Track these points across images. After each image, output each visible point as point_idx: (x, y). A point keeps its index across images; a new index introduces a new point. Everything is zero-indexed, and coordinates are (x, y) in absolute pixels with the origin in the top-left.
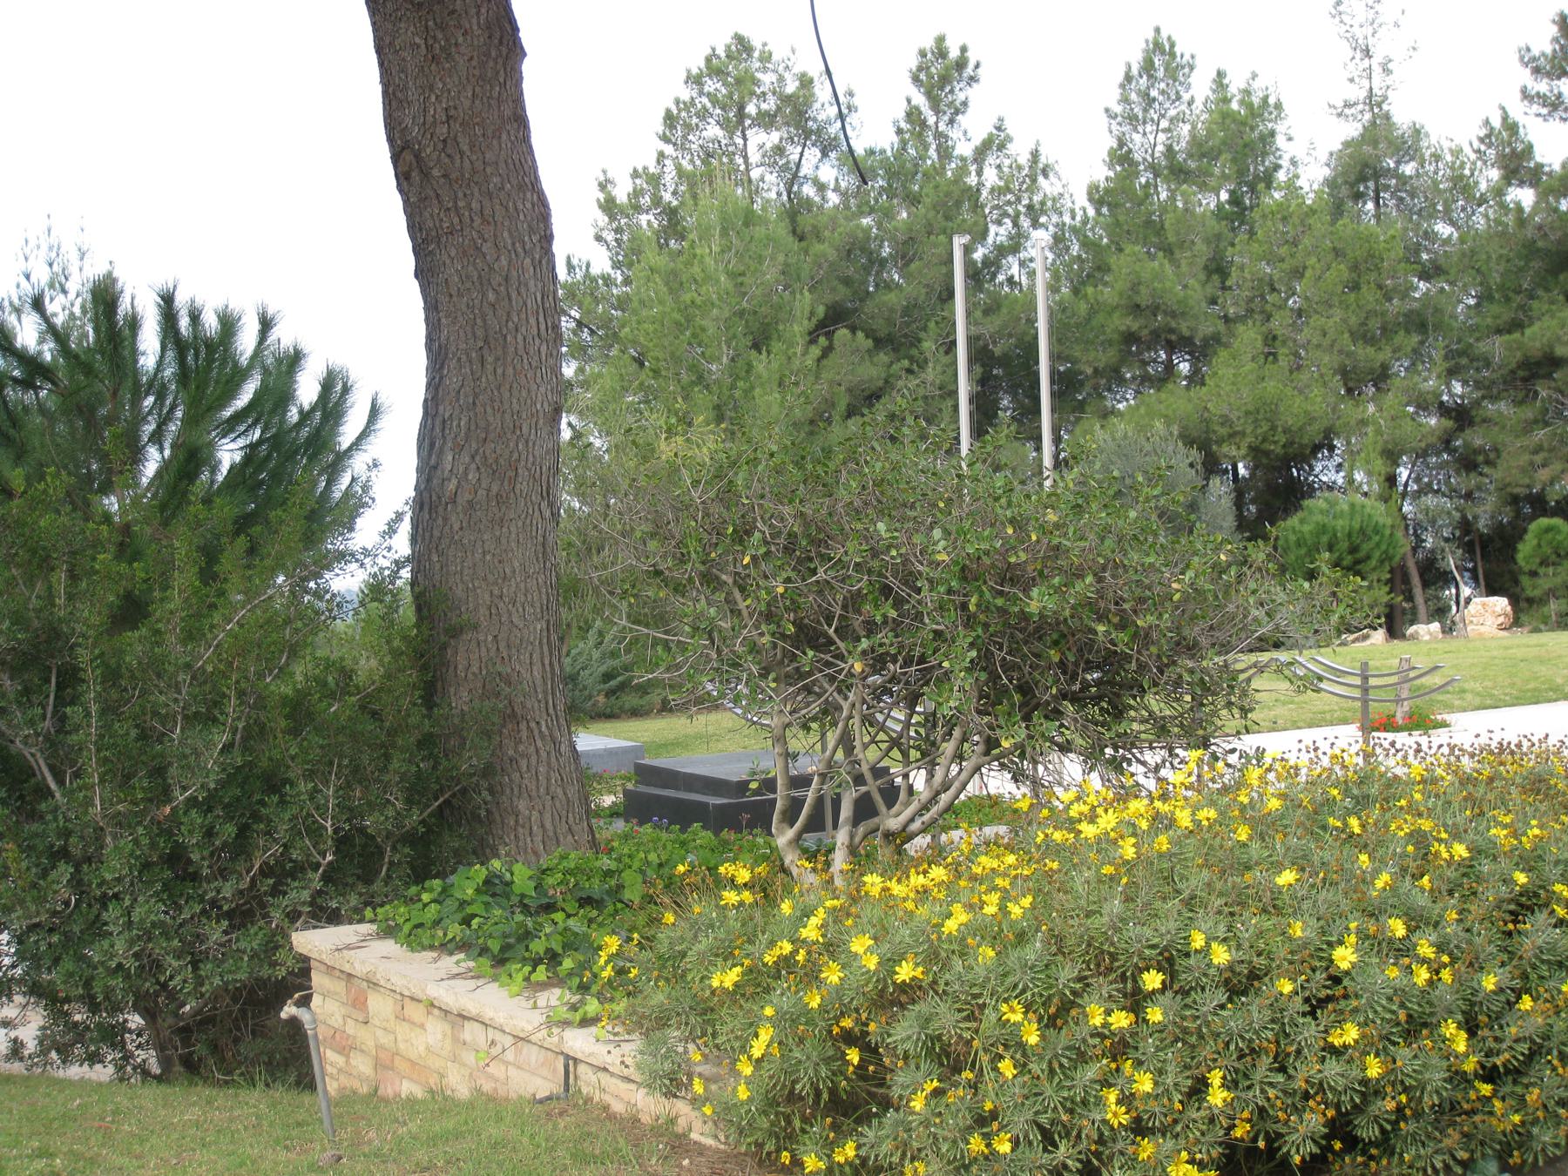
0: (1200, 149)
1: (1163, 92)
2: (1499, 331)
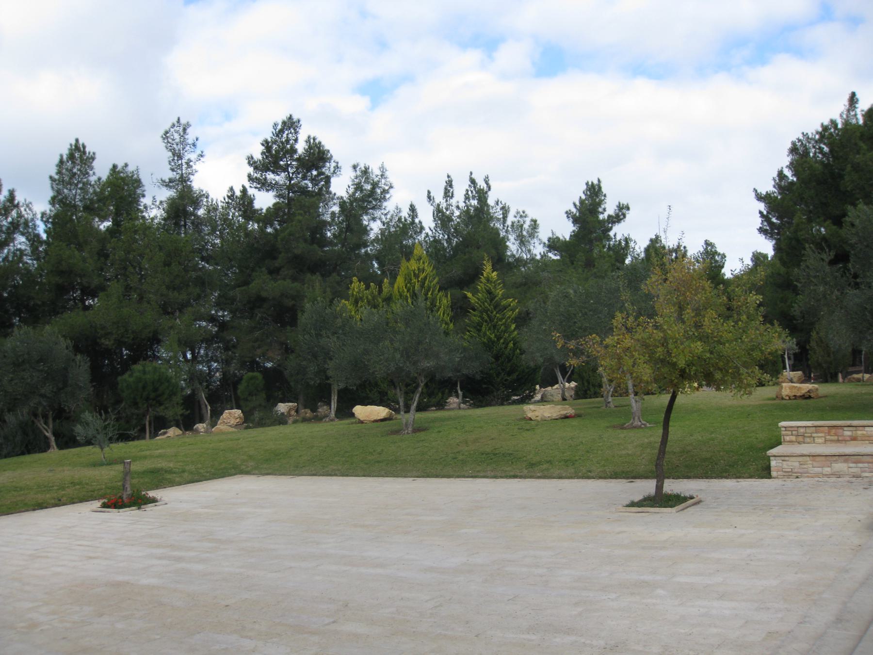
0: (102, 199)
1: (80, 170)
2: (239, 286)
